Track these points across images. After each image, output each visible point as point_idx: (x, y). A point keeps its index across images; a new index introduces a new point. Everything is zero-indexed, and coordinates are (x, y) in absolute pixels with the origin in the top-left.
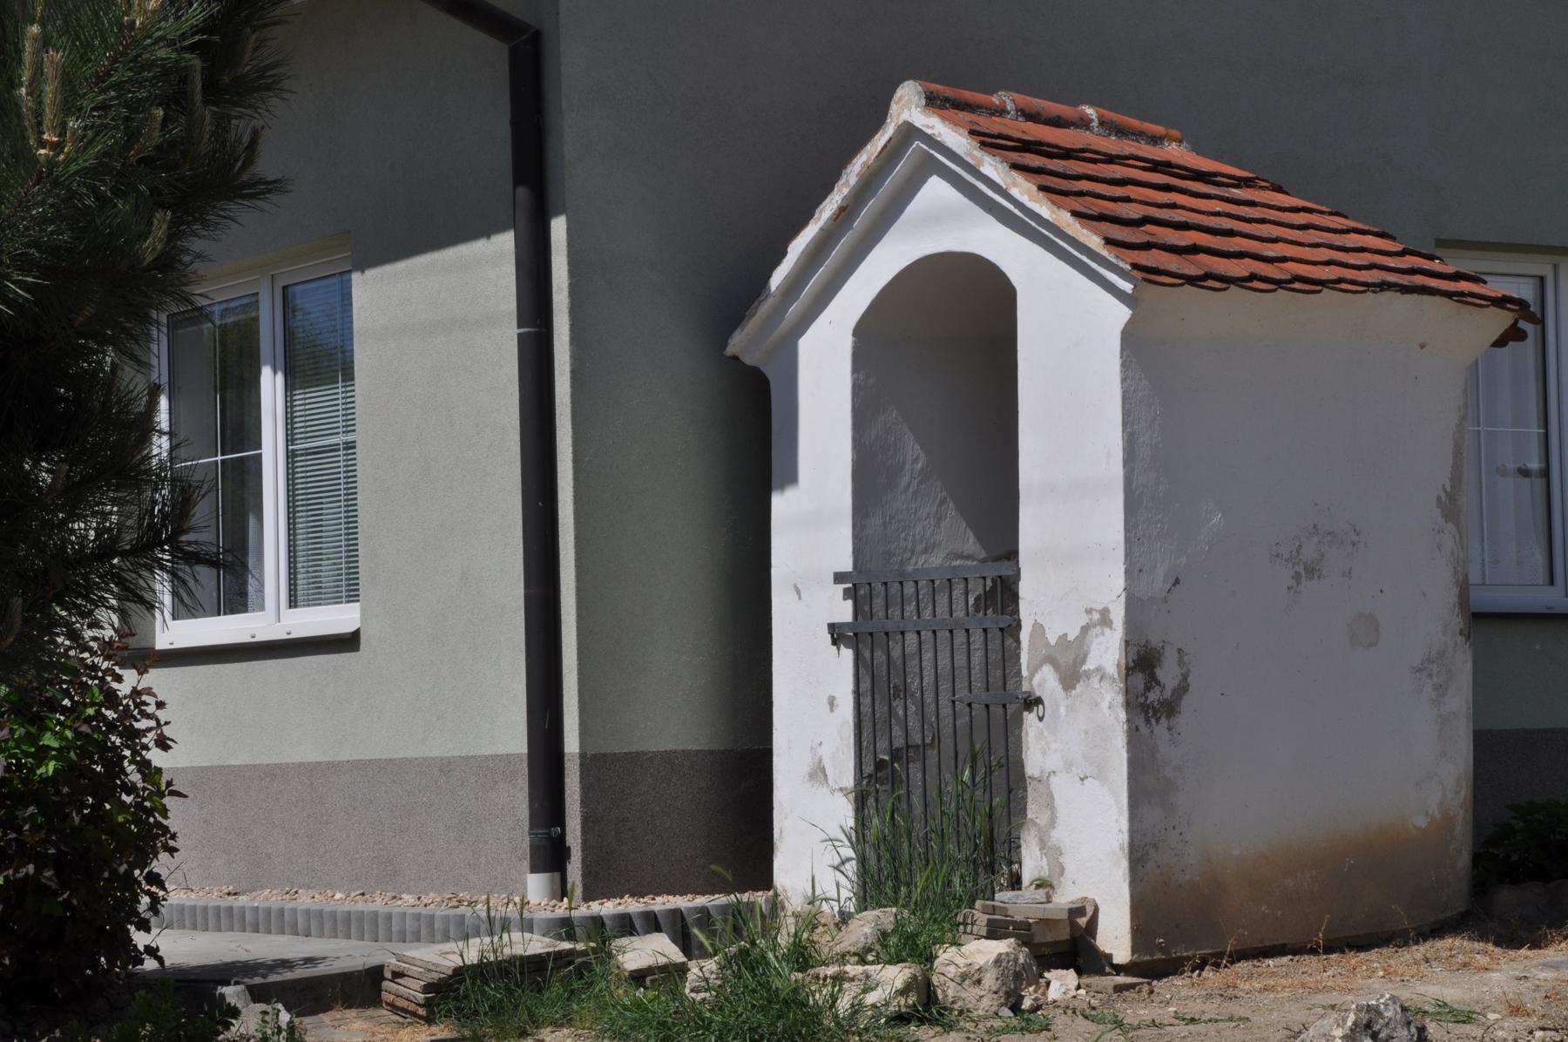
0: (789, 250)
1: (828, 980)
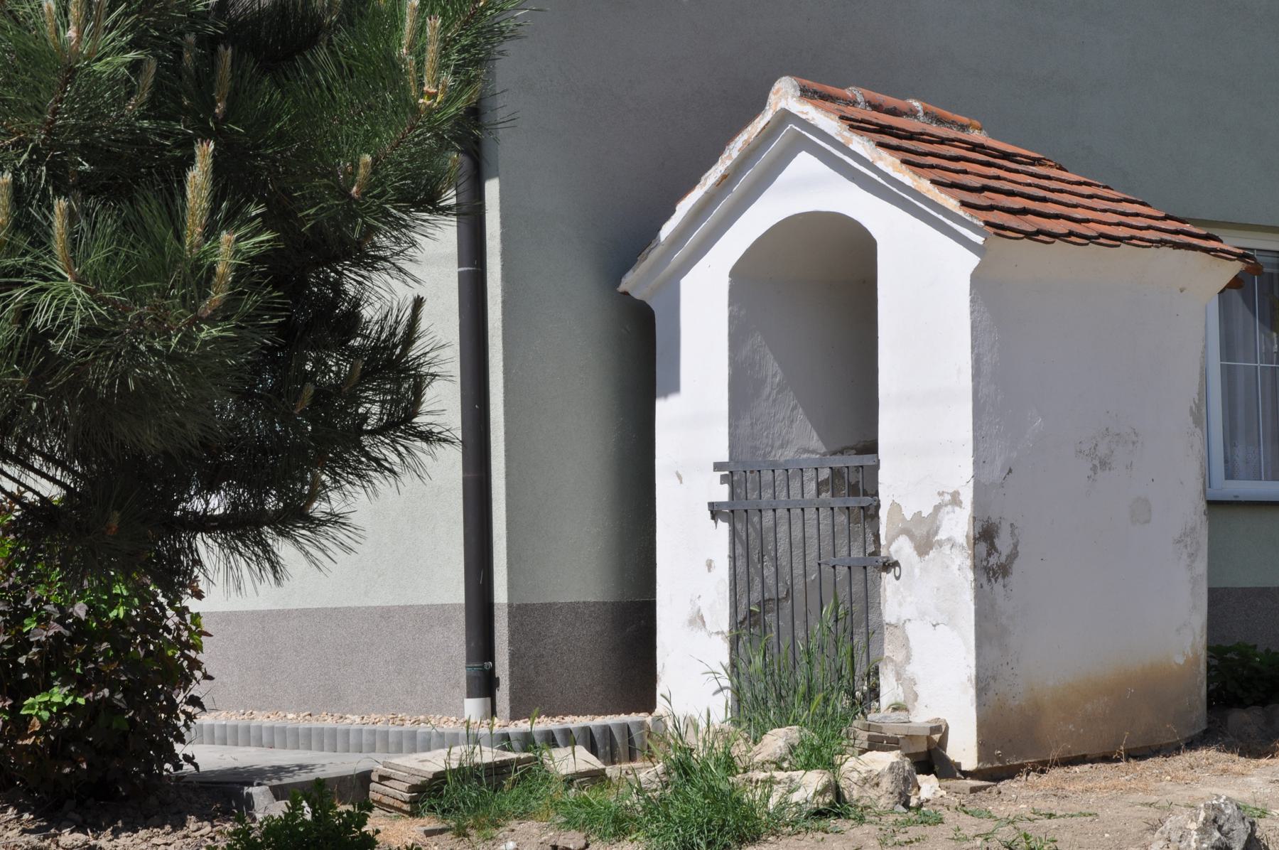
0: (677, 208)
1: (759, 783)
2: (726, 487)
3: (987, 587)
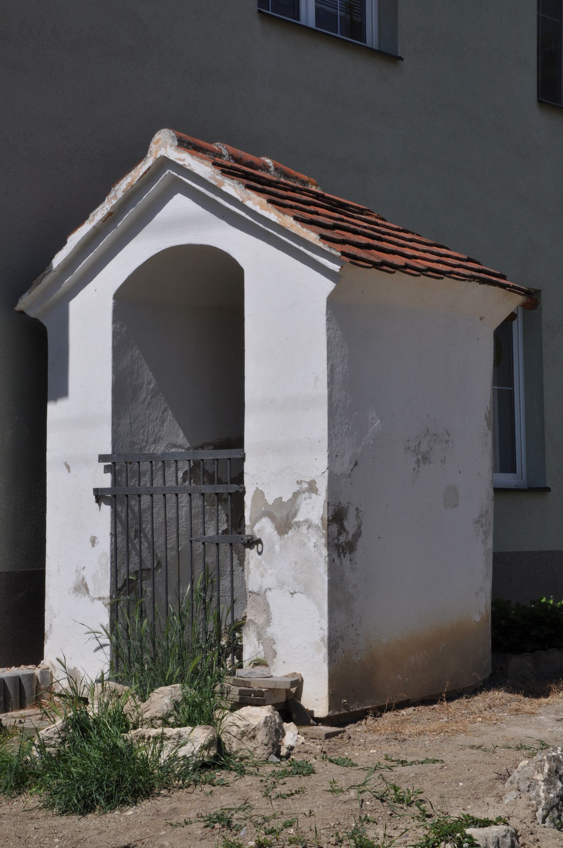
0: (68, 240)
1: (151, 739)
2: (109, 476)
3: (337, 561)
